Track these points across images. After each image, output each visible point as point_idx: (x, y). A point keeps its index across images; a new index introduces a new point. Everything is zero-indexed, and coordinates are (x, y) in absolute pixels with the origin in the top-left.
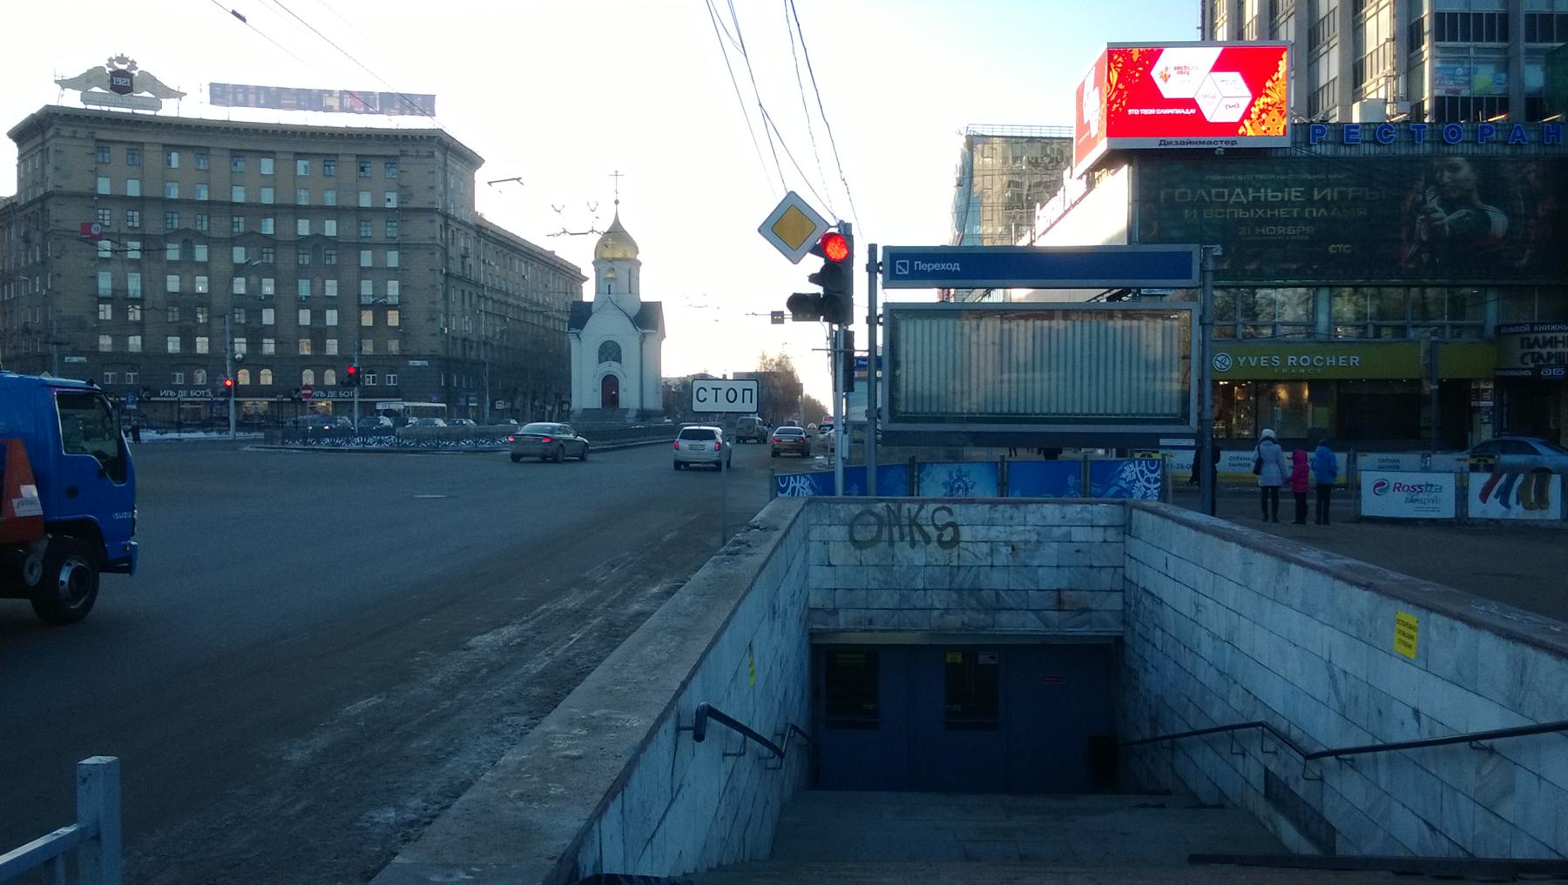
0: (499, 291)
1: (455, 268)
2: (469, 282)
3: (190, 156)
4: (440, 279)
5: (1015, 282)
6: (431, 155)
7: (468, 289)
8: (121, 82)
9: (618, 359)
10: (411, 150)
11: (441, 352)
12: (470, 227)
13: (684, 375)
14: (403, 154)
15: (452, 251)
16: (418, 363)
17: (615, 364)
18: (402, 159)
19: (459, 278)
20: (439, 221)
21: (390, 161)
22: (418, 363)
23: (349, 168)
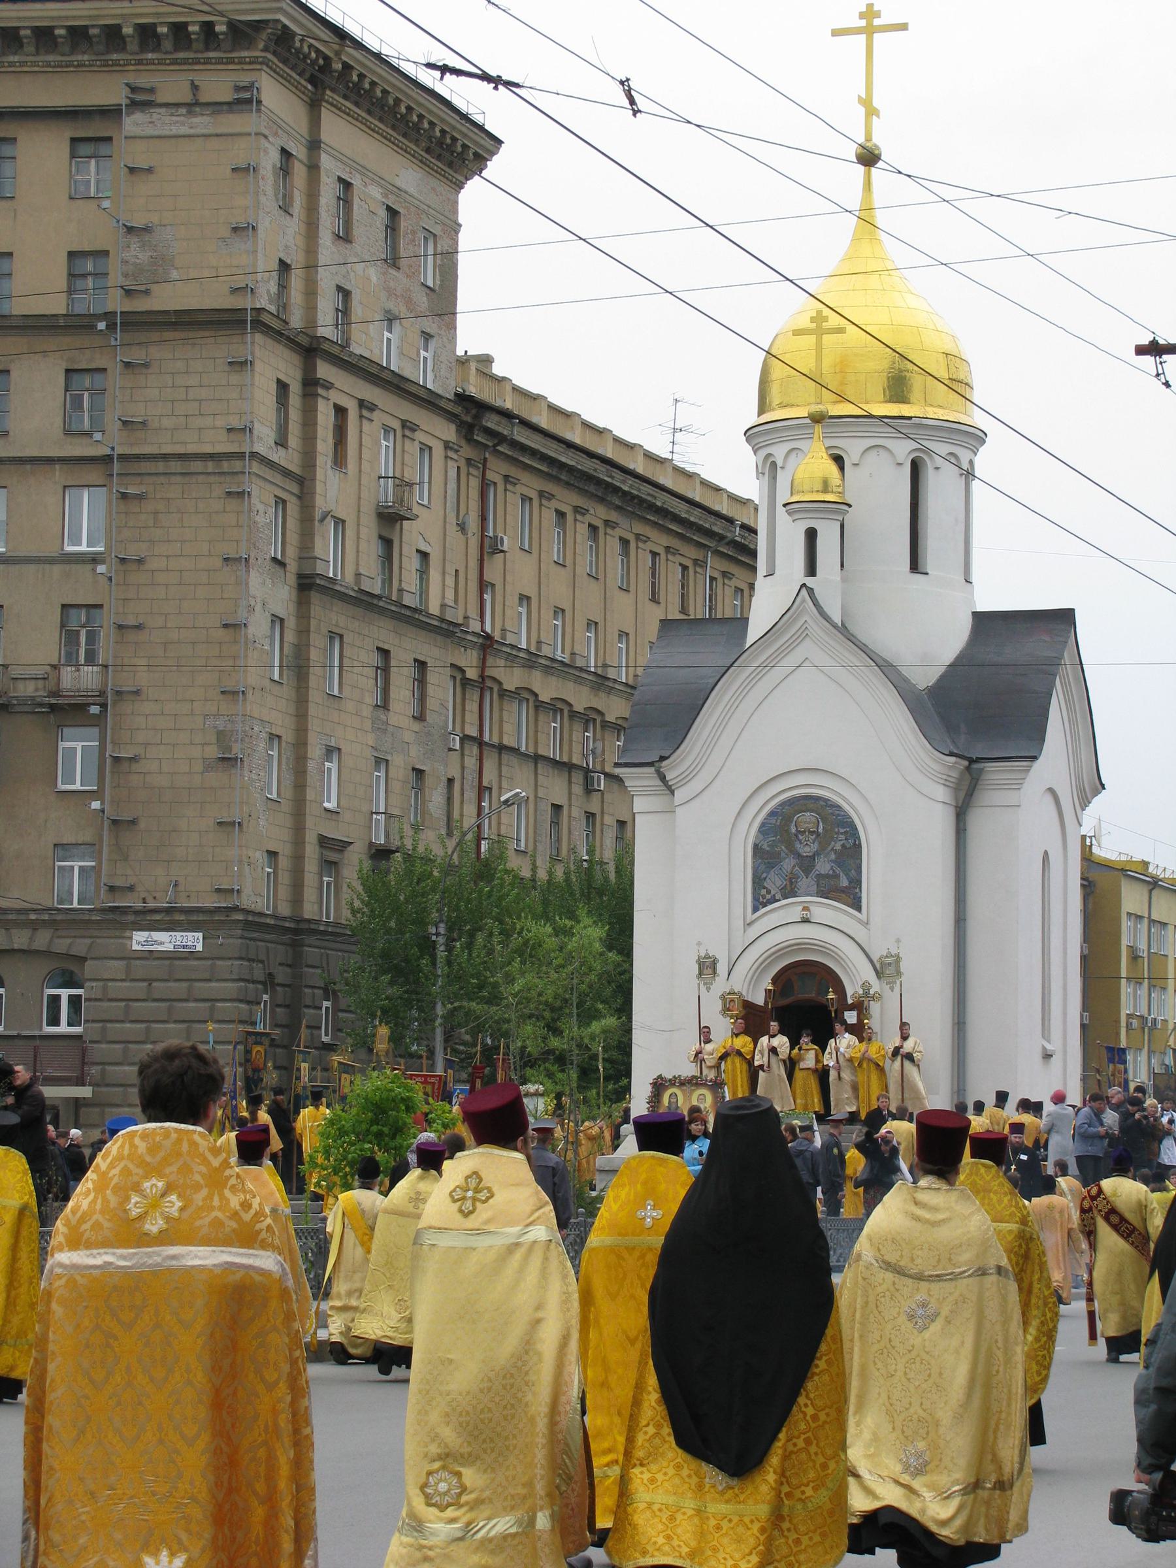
0: (566, 669)
1: (346, 557)
2: (412, 618)
4: (269, 594)
5: (943, 1123)
6: (245, 101)
7: (407, 648)
9: (846, 889)
10: (171, 85)
11: (257, 893)
12: (429, 401)
13: (231, 116)
14: (141, 101)
15: (332, 491)
16: (165, 941)
17: (827, 911)
18: (133, 123)
19: (365, 602)
20: (273, 364)
22: (165, 941)
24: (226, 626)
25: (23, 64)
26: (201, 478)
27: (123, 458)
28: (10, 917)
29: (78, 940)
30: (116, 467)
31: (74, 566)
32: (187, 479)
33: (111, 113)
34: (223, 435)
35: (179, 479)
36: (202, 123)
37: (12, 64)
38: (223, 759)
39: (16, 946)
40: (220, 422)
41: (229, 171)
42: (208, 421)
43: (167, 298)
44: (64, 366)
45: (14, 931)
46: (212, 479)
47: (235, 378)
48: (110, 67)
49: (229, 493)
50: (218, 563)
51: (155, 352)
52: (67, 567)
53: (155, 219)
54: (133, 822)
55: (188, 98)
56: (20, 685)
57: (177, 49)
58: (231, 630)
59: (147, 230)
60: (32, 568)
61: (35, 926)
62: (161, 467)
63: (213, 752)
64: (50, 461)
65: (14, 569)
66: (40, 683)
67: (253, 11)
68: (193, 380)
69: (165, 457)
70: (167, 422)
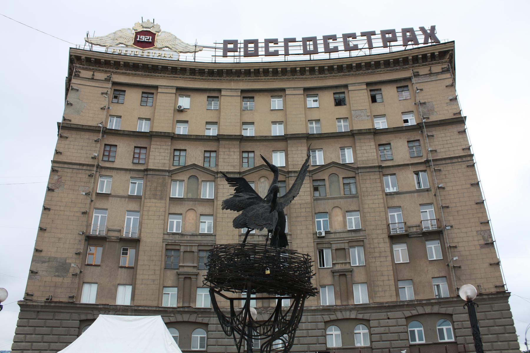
3: (202, 98)
8: (144, 38)
10: (424, 70)
14: (417, 75)
21: (402, 84)
23: (358, 97)
24: (477, 203)
25: (381, 71)
26: (457, 164)
27: (434, 160)
28: (424, 302)
29: (373, 314)
30: (432, 163)
31: (421, 193)
32: (453, 164)
33: (409, 79)
34: (462, 151)
35: (450, 165)
36: (433, 78)
37: (378, 71)
38: (486, 244)
39: (427, 312)
40: (460, 148)
41: (445, 87)
42: (456, 148)
43: (434, 118)
44: (407, 140)
45: (425, 307)
46: (461, 163)
47: (461, 136)
48: (407, 69)
49: (468, 166)
50: (469, 186)
51: (434, 133)
52: (419, 193)
53: (426, 101)
54: (460, 267)
55: (429, 72)
56: (411, 229)
57: (423, 62)
58: (479, 205)
59: (425, 103)
60: (408, 195)
61: (432, 304)
62: (444, 162)
63: (482, 242)
64: (408, 165)
65: (402, 196)
66: (418, 228)
67: (446, 48)
68: (448, 138)
69: (445, 159)
70: (442, 150)
